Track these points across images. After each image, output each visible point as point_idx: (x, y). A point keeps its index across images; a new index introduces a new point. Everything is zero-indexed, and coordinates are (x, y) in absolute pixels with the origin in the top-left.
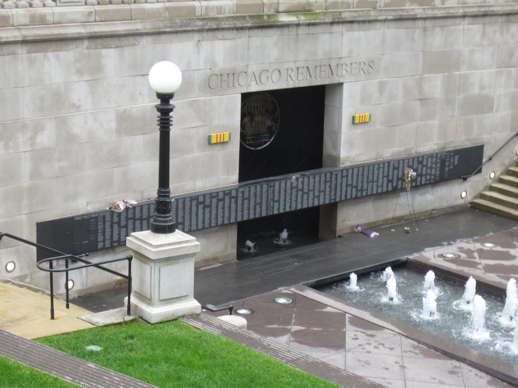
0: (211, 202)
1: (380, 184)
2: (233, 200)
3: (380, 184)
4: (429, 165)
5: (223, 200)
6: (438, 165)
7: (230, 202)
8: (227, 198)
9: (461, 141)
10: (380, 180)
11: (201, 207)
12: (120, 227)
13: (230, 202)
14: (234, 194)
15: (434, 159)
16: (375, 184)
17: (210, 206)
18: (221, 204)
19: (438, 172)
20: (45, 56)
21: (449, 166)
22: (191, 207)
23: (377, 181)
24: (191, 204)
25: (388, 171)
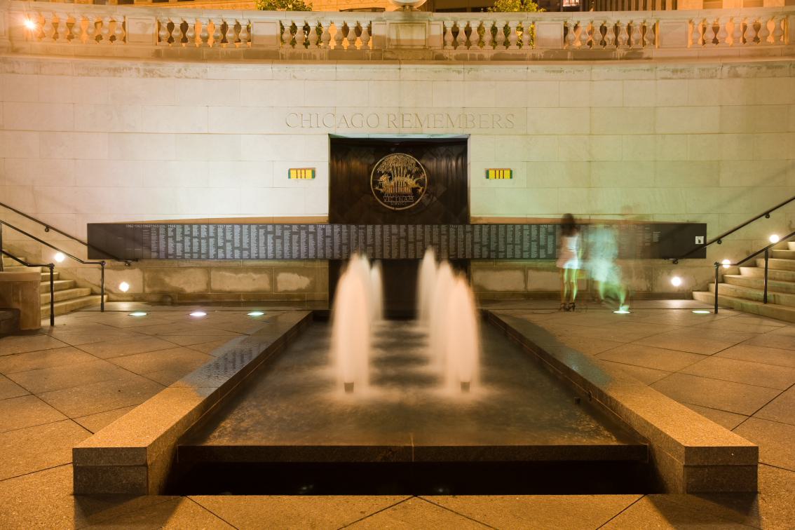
0: (283, 233)
2: (311, 237)
5: (298, 233)
8: (303, 233)
11: (270, 237)
12: (406, 238)
13: (307, 237)
17: (282, 237)
22: (258, 236)
23: (522, 244)
24: (258, 232)
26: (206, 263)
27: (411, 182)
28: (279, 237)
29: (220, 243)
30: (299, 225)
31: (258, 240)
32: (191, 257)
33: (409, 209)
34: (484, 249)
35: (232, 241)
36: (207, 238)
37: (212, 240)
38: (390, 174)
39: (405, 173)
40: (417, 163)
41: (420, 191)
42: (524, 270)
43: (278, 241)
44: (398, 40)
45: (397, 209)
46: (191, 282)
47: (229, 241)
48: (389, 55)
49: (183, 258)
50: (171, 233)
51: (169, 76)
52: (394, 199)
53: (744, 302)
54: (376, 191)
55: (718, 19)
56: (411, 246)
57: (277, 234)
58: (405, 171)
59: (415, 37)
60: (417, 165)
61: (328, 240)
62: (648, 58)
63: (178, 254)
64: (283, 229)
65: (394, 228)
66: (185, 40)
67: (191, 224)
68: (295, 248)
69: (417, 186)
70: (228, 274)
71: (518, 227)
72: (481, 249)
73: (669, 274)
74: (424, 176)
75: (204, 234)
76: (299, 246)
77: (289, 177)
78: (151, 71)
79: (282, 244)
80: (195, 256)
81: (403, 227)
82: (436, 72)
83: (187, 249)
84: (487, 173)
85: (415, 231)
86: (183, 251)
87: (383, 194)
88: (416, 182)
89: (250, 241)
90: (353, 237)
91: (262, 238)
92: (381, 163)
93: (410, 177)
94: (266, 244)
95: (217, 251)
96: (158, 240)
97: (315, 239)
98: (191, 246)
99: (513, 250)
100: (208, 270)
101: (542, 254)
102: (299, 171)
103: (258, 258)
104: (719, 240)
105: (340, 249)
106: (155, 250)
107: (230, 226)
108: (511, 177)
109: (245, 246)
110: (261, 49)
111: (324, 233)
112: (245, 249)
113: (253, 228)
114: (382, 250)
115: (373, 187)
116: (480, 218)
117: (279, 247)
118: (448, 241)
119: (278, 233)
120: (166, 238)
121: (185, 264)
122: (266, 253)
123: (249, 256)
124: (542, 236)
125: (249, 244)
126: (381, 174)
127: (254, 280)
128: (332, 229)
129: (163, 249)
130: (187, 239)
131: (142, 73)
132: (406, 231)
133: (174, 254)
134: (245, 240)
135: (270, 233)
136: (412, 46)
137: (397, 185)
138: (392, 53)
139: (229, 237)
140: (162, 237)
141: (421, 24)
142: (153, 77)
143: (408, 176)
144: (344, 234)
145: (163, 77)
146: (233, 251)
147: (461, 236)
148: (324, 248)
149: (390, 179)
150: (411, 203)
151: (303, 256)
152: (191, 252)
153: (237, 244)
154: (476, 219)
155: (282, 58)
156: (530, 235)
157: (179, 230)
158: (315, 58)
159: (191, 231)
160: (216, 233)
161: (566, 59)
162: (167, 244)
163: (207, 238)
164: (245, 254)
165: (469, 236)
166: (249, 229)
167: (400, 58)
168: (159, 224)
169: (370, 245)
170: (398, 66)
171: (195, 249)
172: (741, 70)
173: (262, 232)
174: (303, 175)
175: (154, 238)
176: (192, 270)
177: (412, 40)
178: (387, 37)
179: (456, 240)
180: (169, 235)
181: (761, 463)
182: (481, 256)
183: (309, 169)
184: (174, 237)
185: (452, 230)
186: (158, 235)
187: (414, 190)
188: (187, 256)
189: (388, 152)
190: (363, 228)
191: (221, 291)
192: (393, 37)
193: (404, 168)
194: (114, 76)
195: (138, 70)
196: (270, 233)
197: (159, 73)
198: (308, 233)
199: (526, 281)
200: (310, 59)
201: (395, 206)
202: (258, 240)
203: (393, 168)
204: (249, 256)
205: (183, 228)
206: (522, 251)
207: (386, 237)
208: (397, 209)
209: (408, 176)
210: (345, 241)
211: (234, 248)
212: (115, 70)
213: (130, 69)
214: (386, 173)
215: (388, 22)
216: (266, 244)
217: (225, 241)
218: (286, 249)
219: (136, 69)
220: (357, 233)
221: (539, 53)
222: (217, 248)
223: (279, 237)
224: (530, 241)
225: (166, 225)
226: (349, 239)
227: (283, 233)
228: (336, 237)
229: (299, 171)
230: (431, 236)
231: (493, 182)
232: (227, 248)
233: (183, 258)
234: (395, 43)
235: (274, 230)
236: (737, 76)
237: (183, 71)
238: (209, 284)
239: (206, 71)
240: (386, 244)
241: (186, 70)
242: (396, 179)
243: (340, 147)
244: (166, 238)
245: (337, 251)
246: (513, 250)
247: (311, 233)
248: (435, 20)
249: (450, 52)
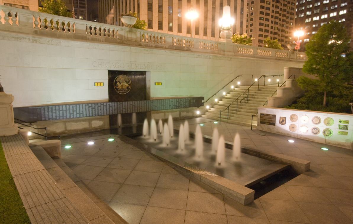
0: (95, 107)
1: (166, 106)
2: (105, 107)
3: (166, 106)
4: (185, 102)
5: (100, 106)
6: (188, 102)
7: (104, 107)
8: (102, 106)
9: (196, 94)
10: (166, 105)
11: (90, 108)
12: (135, 106)
13: (104, 107)
14: (105, 104)
15: (186, 100)
16: (164, 106)
17: (95, 108)
18: (99, 108)
19: (188, 104)
20: (100, 84)
21: (192, 103)
22: (86, 108)
23: (165, 105)
24: (86, 107)
25: (169, 102)
26: (64, 120)
27: (127, 85)
28: (94, 108)
29: (71, 112)
30: (101, 103)
31: (86, 110)
32: (60, 119)
34: (156, 108)
35: (76, 111)
36: (66, 111)
37: (68, 111)
38: (120, 82)
41: (129, 87)
42: (165, 113)
43: (93, 110)
44: (128, 37)
46: (58, 128)
47: (75, 111)
48: (125, 42)
49: (56, 119)
50: (50, 110)
51: (44, 43)
52: (121, 91)
53: (217, 118)
54: (116, 88)
55: (155, 35)
56: (136, 108)
57: (93, 107)
58: (125, 81)
59: (133, 37)
60: (128, 79)
61: (111, 108)
62: (192, 51)
63: (54, 118)
64: (95, 105)
65: (131, 102)
66: (69, 30)
67: (59, 105)
68: (99, 112)
70: (73, 123)
71: (261, 118)
72: (155, 108)
73: (197, 111)
74: (130, 82)
75: (64, 109)
76: (101, 111)
77: (95, 85)
78: (36, 40)
79: (95, 110)
80: (62, 118)
81: (134, 102)
82: (141, 50)
83: (58, 115)
84: (155, 83)
85: (137, 103)
86: (56, 116)
87: (118, 89)
89: (83, 110)
90: (119, 106)
91: (87, 109)
94: (89, 111)
95: (70, 115)
96: (45, 113)
97: (106, 108)
98: (59, 114)
99: (163, 107)
100: (65, 122)
101: (170, 108)
102: (98, 83)
103: (86, 116)
104: (206, 101)
105: (115, 111)
106: (44, 117)
107: (75, 105)
108: (161, 85)
109: (81, 112)
110: (80, 35)
111: (109, 106)
112: (81, 114)
113: (84, 105)
114: (128, 110)
116: (153, 98)
117: (94, 111)
118: (146, 106)
119: (93, 107)
120: (48, 112)
121: (56, 121)
122: (89, 114)
123: (83, 116)
124: (170, 103)
125: (83, 111)
127: (83, 124)
128: (112, 104)
129: (47, 116)
130: (57, 112)
131: (31, 41)
132: (135, 103)
133: (52, 118)
134: (81, 110)
135: (90, 107)
136: (132, 40)
137: (122, 86)
138: (126, 42)
139: (75, 109)
140: (46, 112)
141: (135, 33)
142: (37, 43)
143: (126, 83)
144: (116, 106)
145: (41, 43)
146: (77, 115)
147: (150, 104)
148: (109, 111)
149: (120, 84)
150: (126, 92)
151: (102, 114)
152: (60, 117)
153: (78, 112)
154: (152, 98)
155: (89, 40)
156: (167, 103)
157: (54, 108)
158: (100, 41)
159: (59, 108)
160: (70, 108)
161: (173, 49)
162: (49, 114)
163: (66, 111)
164: (81, 115)
165: (152, 103)
166: (83, 106)
167: (129, 44)
168: (45, 106)
169: (124, 109)
170: (130, 47)
171: (61, 115)
172: (211, 57)
173: (87, 107)
174: (100, 85)
175: (43, 112)
176: (58, 123)
177: (132, 38)
178: (124, 35)
179: (149, 105)
180: (49, 110)
182: (153, 110)
183: (102, 82)
184: (52, 111)
185: (147, 102)
186: (44, 110)
187: (128, 87)
188: (58, 118)
189: (121, 74)
190: (122, 103)
191: (70, 130)
192: (126, 36)
194: (18, 41)
195: (29, 39)
196: (90, 107)
197: (39, 41)
198: (104, 106)
199: (165, 116)
200: (99, 41)
202: (86, 110)
204: (83, 116)
205: (56, 107)
206: (165, 107)
207: (129, 106)
208: (123, 94)
209: (126, 83)
210: (116, 108)
211: (77, 114)
212: (18, 38)
213: (25, 38)
214: (119, 81)
215: (124, 30)
216: (89, 111)
217: (73, 111)
218: (96, 112)
219: (28, 38)
220: (120, 105)
221: (167, 46)
222: (70, 114)
223: (94, 108)
224: (167, 104)
225: (48, 106)
226: (117, 107)
227: (95, 107)
228: (113, 107)
229: (98, 83)
230: (142, 104)
231: (157, 86)
232: (74, 114)
233: (56, 119)
234: (126, 38)
235: (92, 105)
236: (210, 58)
237: (50, 41)
238: (66, 128)
239: (60, 43)
240: (129, 108)
241: (51, 41)
242: (122, 84)
243: (111, 73)
244: (48, 112)
245: (114, 112)
246: (163, 107)
247: (105, 106)
248: (138, 32)
249: (89, 36)
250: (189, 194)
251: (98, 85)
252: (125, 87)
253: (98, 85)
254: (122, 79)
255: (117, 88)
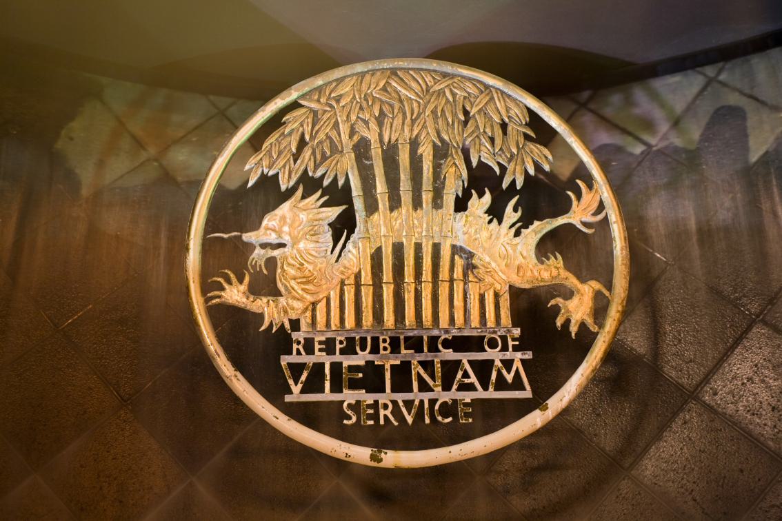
27: (507, 253)
33: (493, 458)
38: (338, 195)
39: (452, 189)
40: (535, 121)
45: (393, 458)
52: (371, 379)
69: (553, 270)
87: (281, 340)
88: (546, 246)
92: (275, 122)
93: (496, 212)
115: (207, 287)
126: (270, 193)
143: (480, 204)
149: (344, 227)
181: (370, 285)
187: (532, 310)
193: (441, 152)
201: (382, 438)
203: (362, 150)
208: (393, 458)
209: (480, 204)
214: (309, 184)
242: (381, 228)
250: (699, 372)
251: (427, 197)
252: (477, 306)
253: (427, 197)
254: (400, 133)
255: (271, 312)
